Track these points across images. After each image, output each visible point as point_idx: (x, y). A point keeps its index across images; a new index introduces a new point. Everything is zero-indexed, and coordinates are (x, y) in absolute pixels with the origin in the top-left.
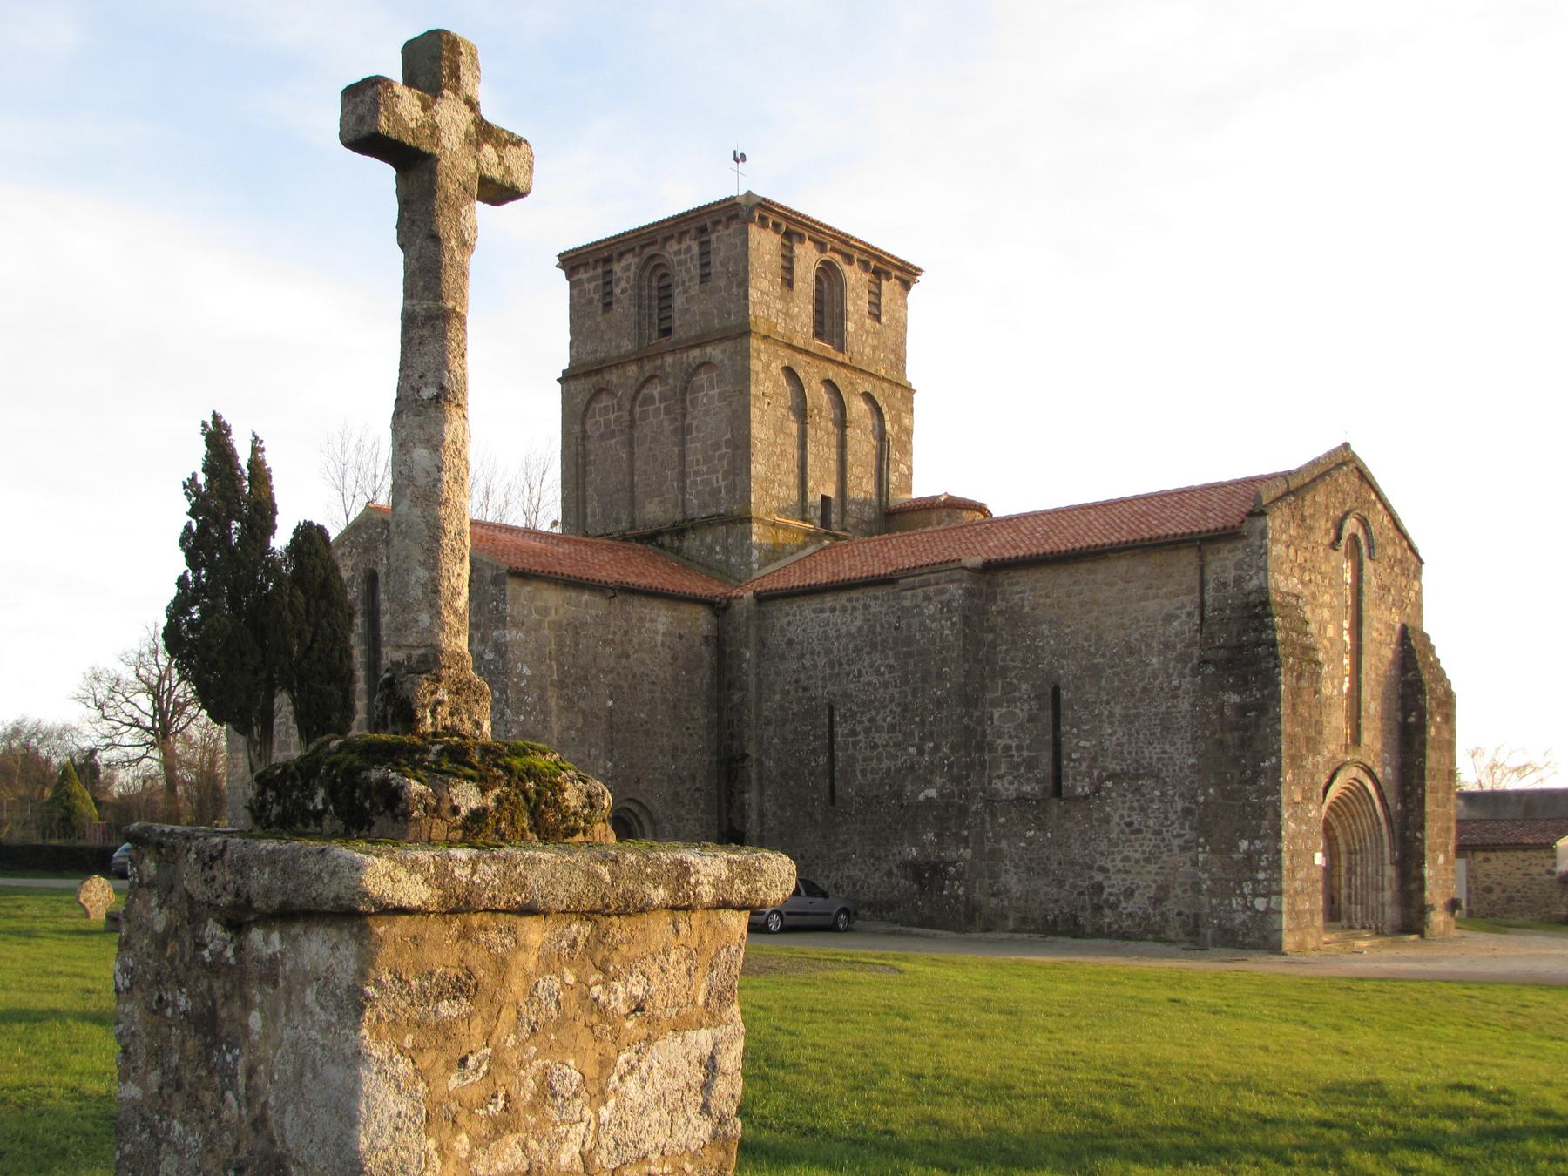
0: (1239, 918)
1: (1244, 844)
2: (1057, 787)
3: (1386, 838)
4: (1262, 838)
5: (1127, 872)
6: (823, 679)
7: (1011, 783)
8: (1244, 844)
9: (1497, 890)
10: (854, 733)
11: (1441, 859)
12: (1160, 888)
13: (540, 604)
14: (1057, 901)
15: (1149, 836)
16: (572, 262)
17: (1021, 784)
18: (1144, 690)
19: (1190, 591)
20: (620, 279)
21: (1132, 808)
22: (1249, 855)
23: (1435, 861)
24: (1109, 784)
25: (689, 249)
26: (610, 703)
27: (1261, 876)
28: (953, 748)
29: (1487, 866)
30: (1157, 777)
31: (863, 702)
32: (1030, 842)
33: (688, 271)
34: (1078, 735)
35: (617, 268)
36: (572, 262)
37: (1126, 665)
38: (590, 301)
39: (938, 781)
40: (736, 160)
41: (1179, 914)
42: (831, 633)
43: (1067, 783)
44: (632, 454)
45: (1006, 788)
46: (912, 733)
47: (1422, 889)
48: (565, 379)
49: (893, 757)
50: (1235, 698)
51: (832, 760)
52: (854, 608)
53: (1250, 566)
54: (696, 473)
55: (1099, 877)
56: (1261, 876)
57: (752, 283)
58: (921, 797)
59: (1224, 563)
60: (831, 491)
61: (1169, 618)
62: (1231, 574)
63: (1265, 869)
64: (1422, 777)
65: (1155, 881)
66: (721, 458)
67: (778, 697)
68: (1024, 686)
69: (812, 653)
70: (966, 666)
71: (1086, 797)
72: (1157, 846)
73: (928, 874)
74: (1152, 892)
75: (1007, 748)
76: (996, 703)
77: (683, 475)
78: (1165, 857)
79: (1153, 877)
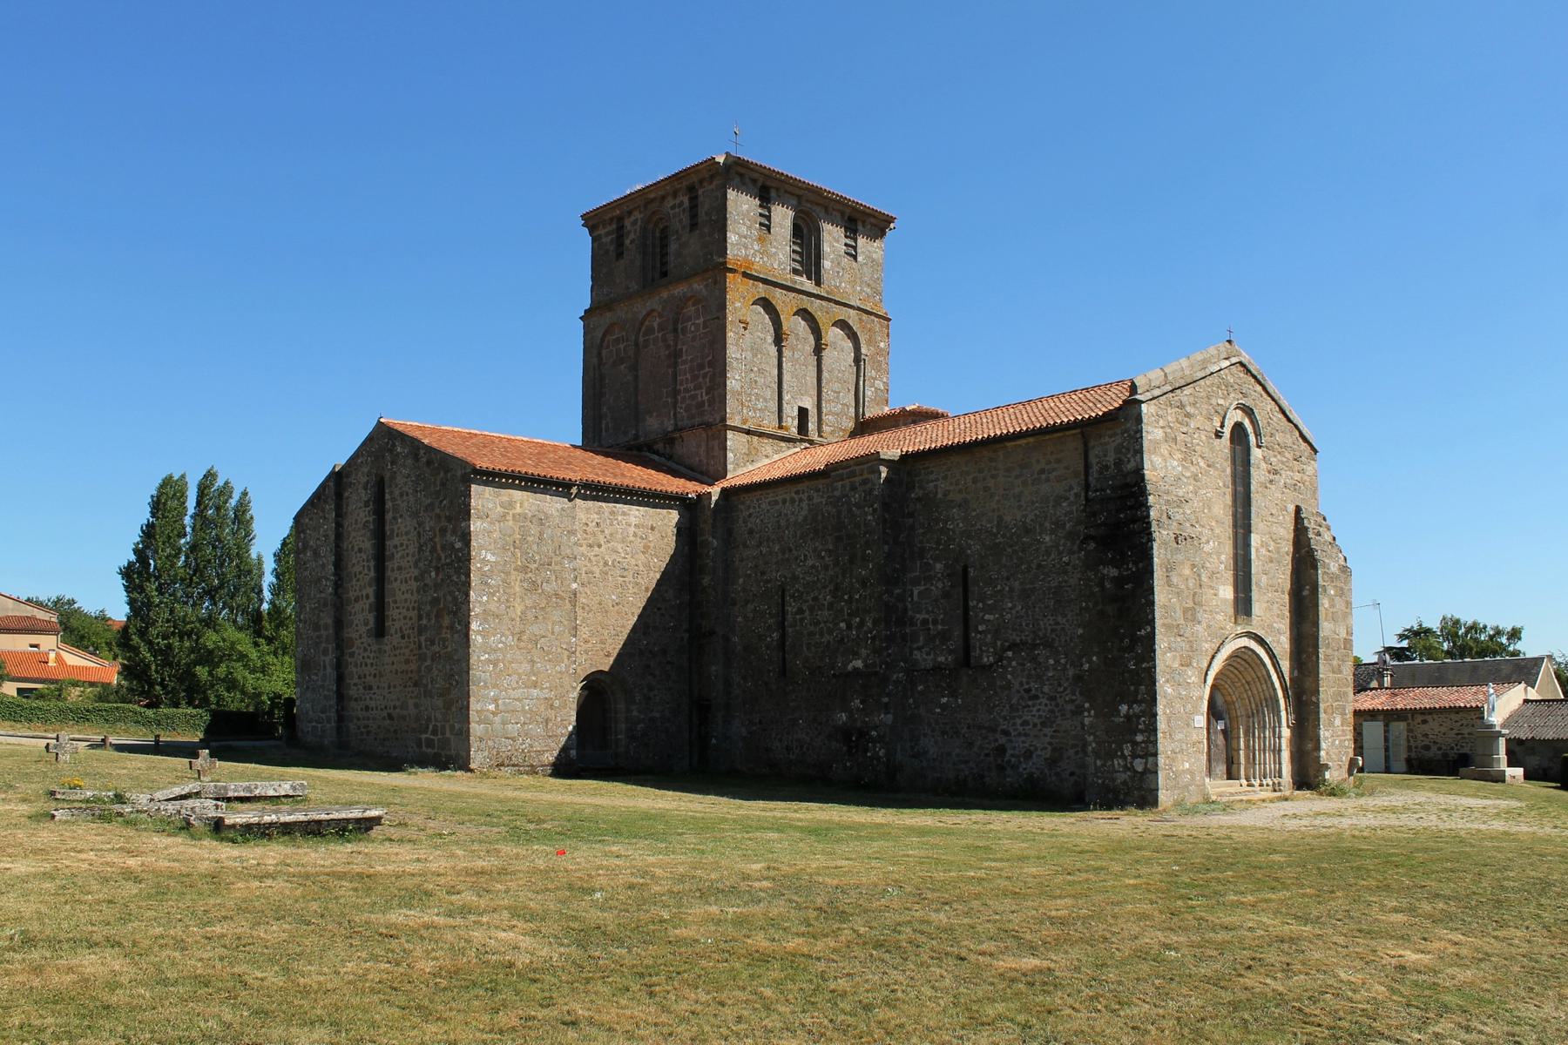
0: (1122, 777)
1: (1124, 708)
2: (965, 658)
3: (1282, 702)
4: (1139, 702)
5: (1026, 735)
7: (928, 654)
8: (1124, 708)
9: (1434, 749)
10: (800, 611)
11: (1338, 722)
12: (1054, 750)
14: (967, 762)
15: (1044, 701)
16: (593, 221)
18: (1039, 566)
22: (1128, 717)
23: (1331, 724)
24: (1010, 654)
25: (681, 203)
27: (1139, 738)
28: (875, 622)
29: (1425, 728)
32: (944, 707)
34: (982, 610)
35: (627, 223)
38: (607, 252)
39: (864, 652)
41: (1072, 774)
42: (783, 523)
43: (975, 653)
44: (636, 377)
45: (923, 658)
46: (842, 610)
47: (1318, 748)
48: (587, 316)
49: (830, 632)
50: (1114, 572)
51: (783, 636)
54: (686, 390)
55: (1003, 740)
56: (1139, 738)
57: (730, 228)
58: (850, 667)
60: (809, 403)
62: (1111, 458)
63: (1142, 732)
64: (1316, 647)
66: (705, 376)
68: (938, 566)
70: (886, 548)
71: (991, 665)
72: (1052, 711)
73: (854, 738)
74: (1048, 754)
75: (925, 622)
76: (915, 582)
77: (675, 393)
78: (1059, 721)
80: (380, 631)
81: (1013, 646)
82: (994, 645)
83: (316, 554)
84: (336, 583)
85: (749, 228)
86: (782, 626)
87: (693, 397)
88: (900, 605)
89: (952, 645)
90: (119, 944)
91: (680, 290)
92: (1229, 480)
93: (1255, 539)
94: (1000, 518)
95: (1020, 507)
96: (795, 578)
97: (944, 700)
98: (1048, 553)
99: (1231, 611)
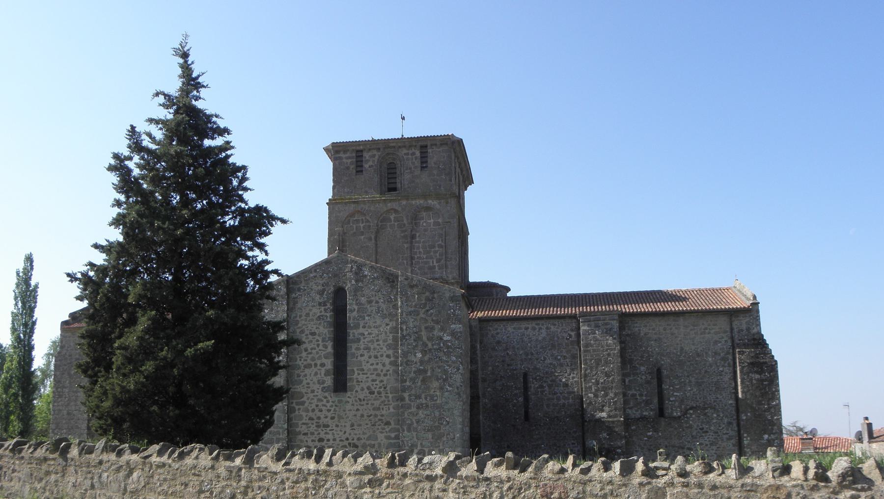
2: (661, 412)
4: (774, 434)
6: (522, 360)
8: (766, 436)
16: (336, 151)
18: (706, 372)
19: (725, 332)
21: (703, 422)
22: (768, 440)
24: (691, 412)
28: (616, 394)
30: (714, 409)
31: (547, 373)
32: (650, 437)
34: (673, 390)
36: (336, 151)
52: (540, 329)
59: (742, 323)
61: (716, 342)
62: (744, 327)
67: (490, 368)
68: (642, 368)
69: (514, 347)
71: (680, 417)
75: (634, 395)
80: (340, 384)
82: (680, 407)
89: (652, 406)
94: (682, 349)
95: (693, 344)
98: (711, 366)
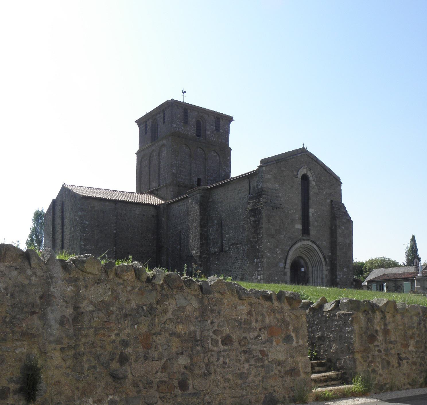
1: (256, 260)
2: (222, 250)
10: (184, 239)
12: (242, 275)
13: (92, 205)
17: (215, 249)
18: (239, 219)
20: (148, 126)
22: (256, 263)
24: (231, 247)
26: (115, 231)
32: (217, 265)
33: (161, 121)
35: (148, 123)
37: (235, 213)
40: (183, 93)
42: (181, 212)
45: (212, 250)
53: (260, 182)
56: (259, 269)
62: (255, 185)
63: (260, 267)
65: (241, 274)
68: (216, 221)
71: (227, 251)
72: (241, 263)
75: (213, 239)
79: (240, 272)
81: (232, 244)
83: (48, 226)
84: (53, 234)
85: (180, 122)
86: (180, 244)
87: (164, 176)
88: (206, 234)
90: (156, 373)
91: (161, 143)
92: (300, 192)
93: (311, 211)
94: (230, 206)
96: (183, 228)
97: (217, 262)
98: (241, 215)
99: (301, 232)
